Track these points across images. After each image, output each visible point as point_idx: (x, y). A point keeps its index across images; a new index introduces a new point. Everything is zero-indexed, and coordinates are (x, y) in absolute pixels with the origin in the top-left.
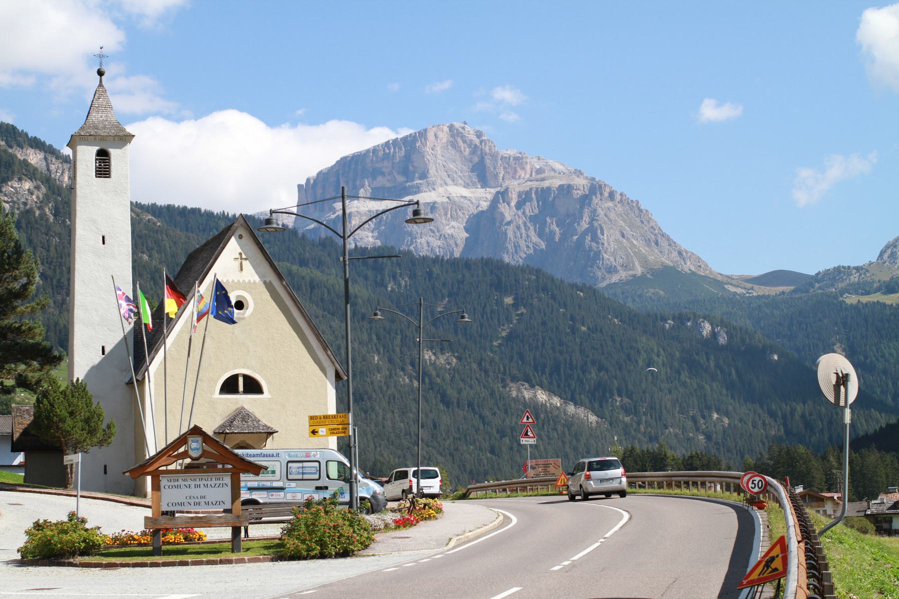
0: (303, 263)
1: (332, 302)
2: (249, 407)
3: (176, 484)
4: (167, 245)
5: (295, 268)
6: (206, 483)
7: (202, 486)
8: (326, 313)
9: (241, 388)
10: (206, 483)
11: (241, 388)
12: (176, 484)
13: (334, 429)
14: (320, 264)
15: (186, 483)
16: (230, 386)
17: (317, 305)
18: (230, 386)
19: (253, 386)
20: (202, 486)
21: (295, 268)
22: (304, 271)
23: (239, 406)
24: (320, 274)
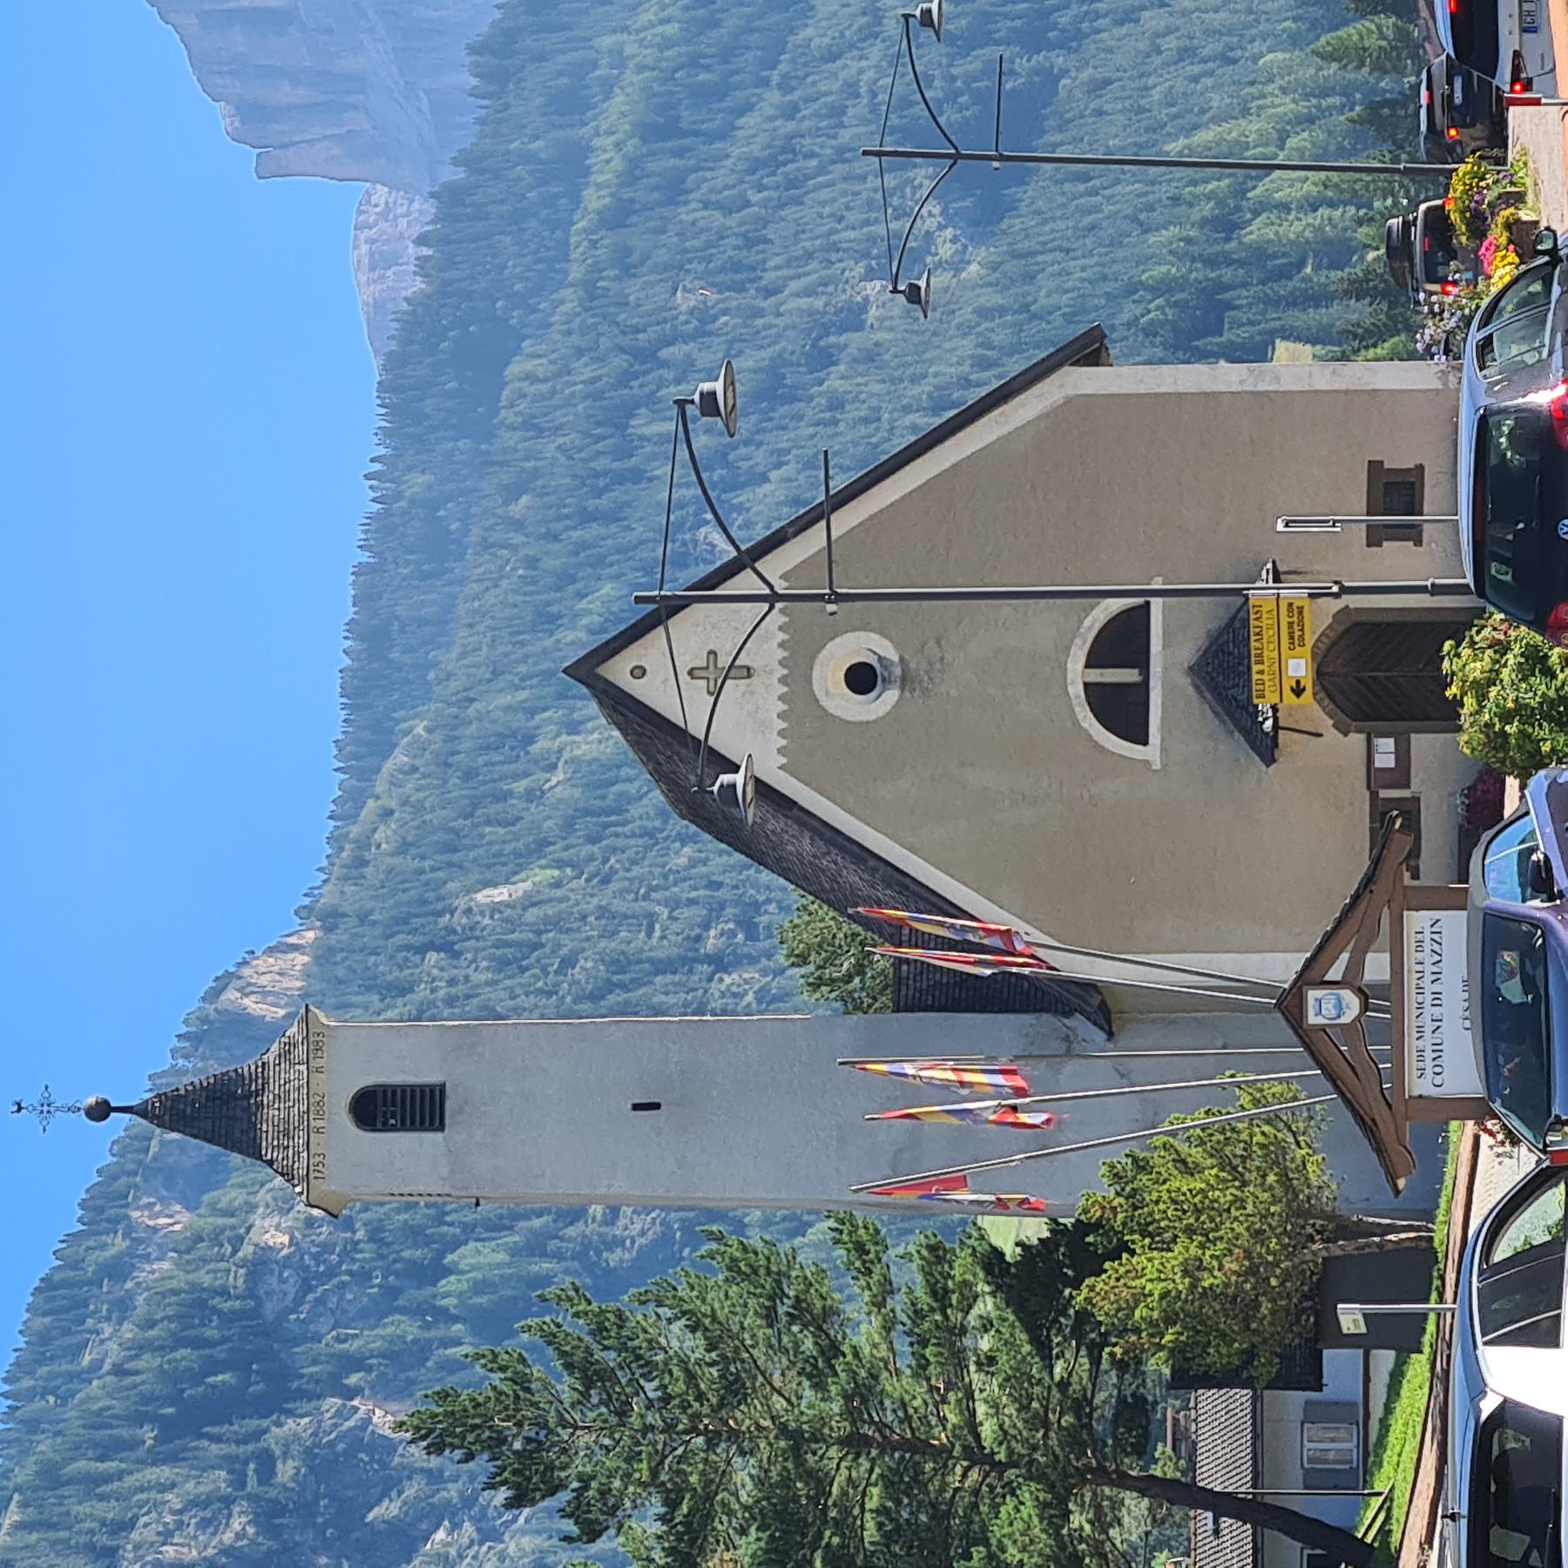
0: (572, 166)
1: (728, 53)
2: (1188, 653)
3: (1429, 1055)
4: (507, 699)
5: (594, 200)
6: (1429, 977)
7: (1436, 987)
8: (775, 77)
9: (1130, 676)
10: (1429, 977)
11: (1130, 676)
12: (1429, 1055)
13: (1292, 637)
14: (572, 103)
15: (1428, 1030)
16: (1123, 711)
17: (746, 108)
18: (1123, 711)
19: (1124, 641)
20: (1436, 987)
21: (594, 200)
22: (606, 165)
23: (1185, 682)
24: (619, 99)
